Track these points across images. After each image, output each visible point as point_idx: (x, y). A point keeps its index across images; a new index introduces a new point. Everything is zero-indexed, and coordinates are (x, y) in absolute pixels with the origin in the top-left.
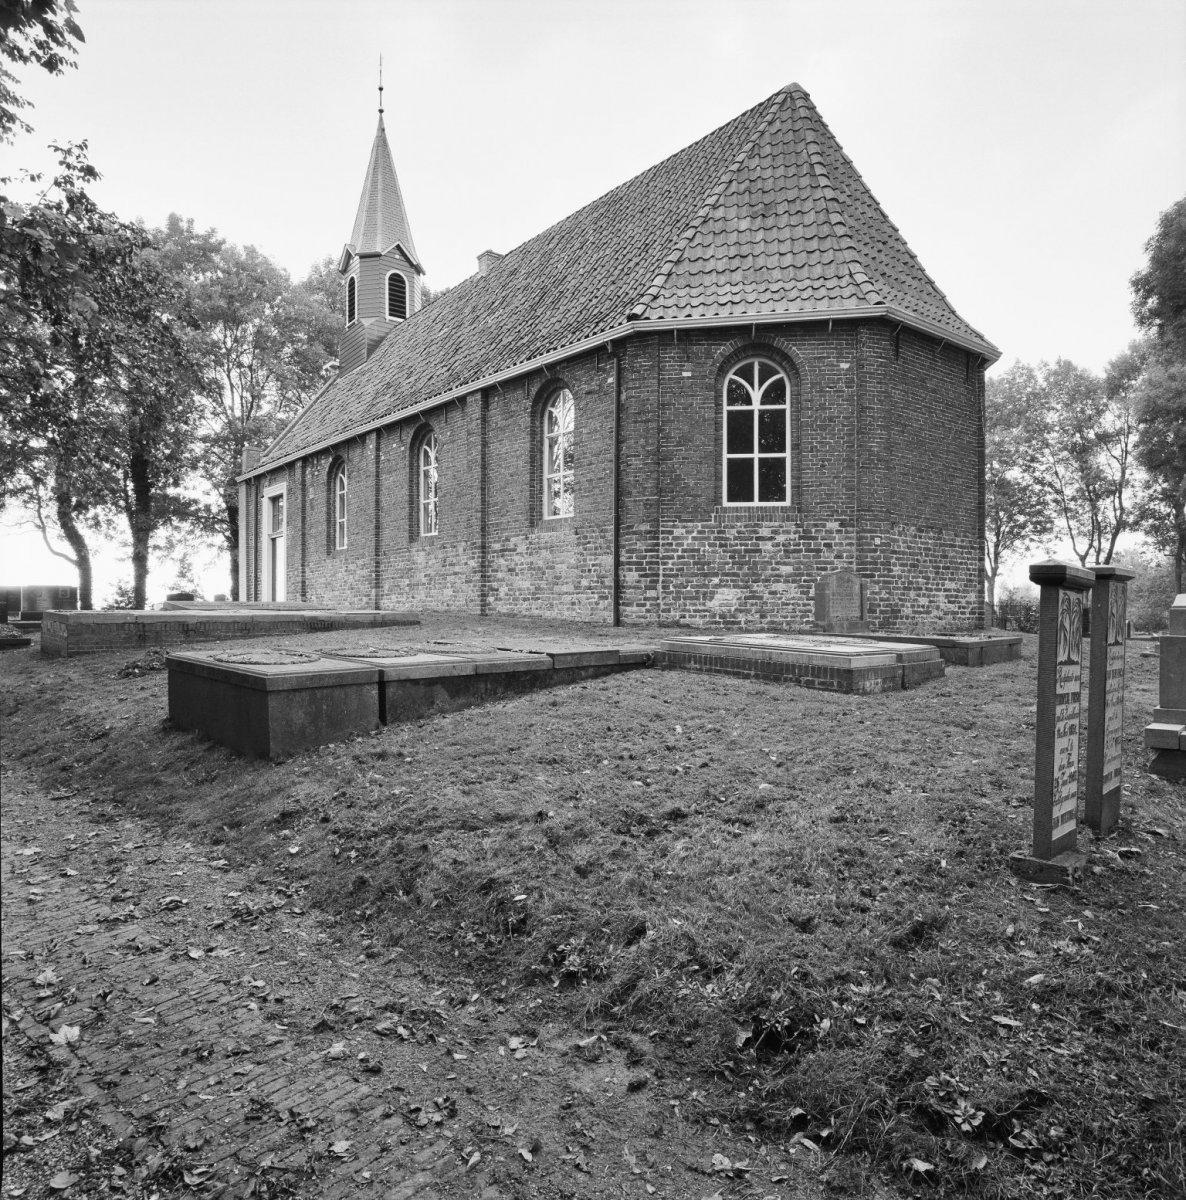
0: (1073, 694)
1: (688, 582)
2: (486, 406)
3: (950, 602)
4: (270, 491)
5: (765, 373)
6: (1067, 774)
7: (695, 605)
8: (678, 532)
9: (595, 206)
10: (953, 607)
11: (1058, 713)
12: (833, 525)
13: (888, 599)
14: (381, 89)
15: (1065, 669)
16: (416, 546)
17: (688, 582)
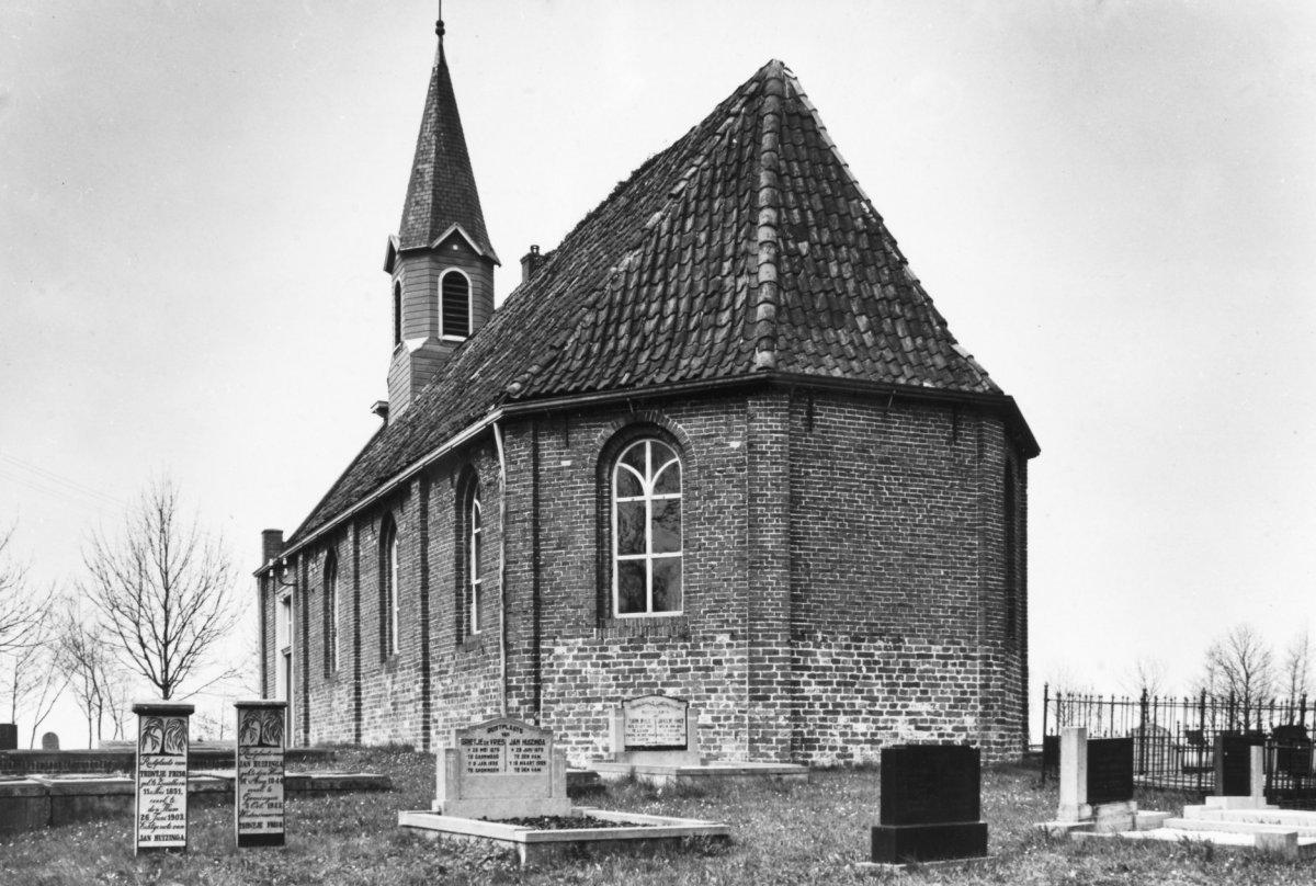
1: (570, 709)
3: (918, 728)
8: (559, 650)
12: (724, 639)
17: (570, 709)
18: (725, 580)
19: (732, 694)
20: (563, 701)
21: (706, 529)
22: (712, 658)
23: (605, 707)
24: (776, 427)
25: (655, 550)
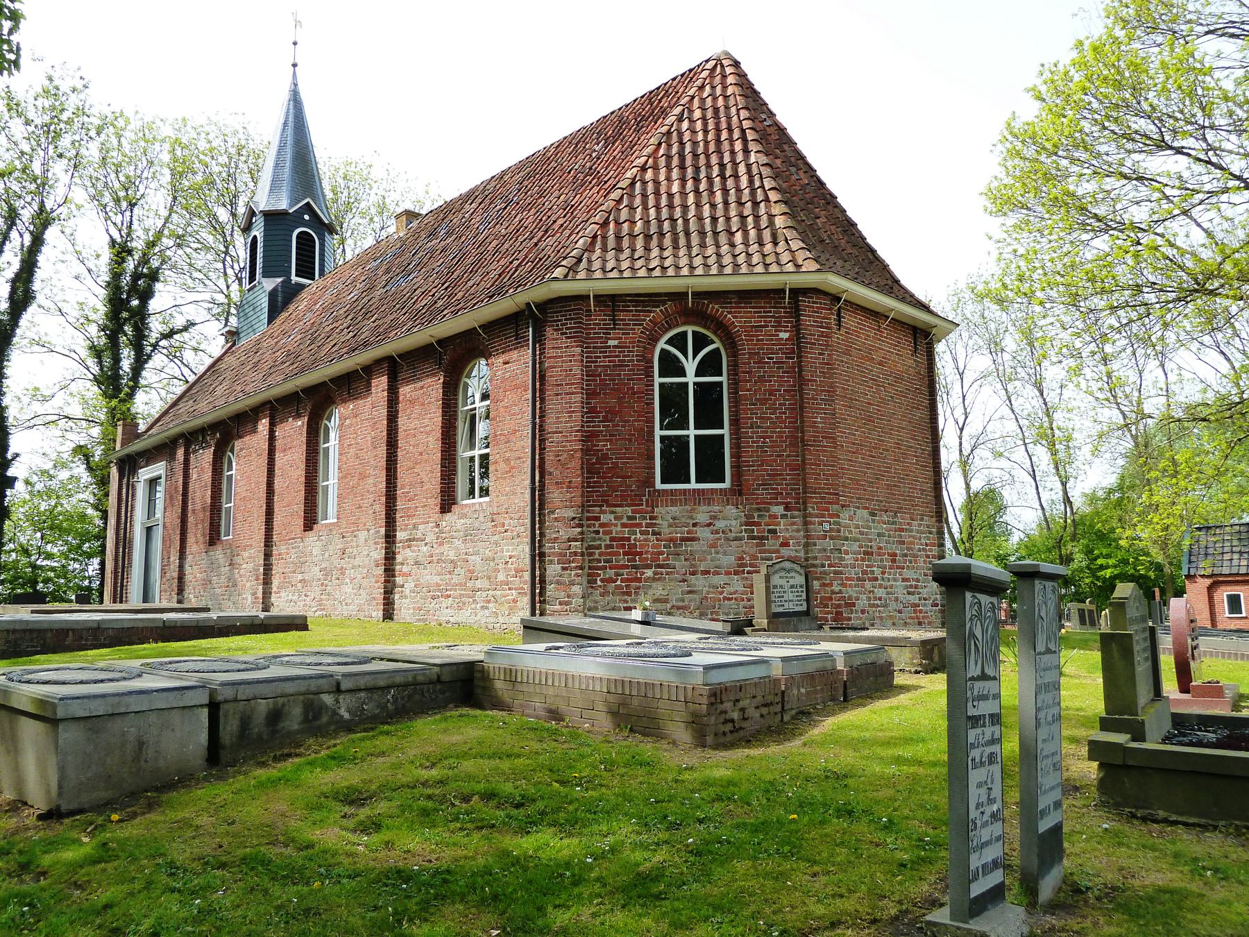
0: (992, 716)
3: (909, 593)
4: (145, 474)
5: (700, 342)
6: (988, 813)
7: (626, 601)
9: (521, 166)
10: (914, 599)
11: (971, 739)
12: (778, 510)
13: (840, 592)
14: (295, 44)
15: (978, 685)
16: (311, 537)
18: (778, 456)
20: (610, 568)
21: (758, 409)
22: (767, 528)
23: (655, 573)
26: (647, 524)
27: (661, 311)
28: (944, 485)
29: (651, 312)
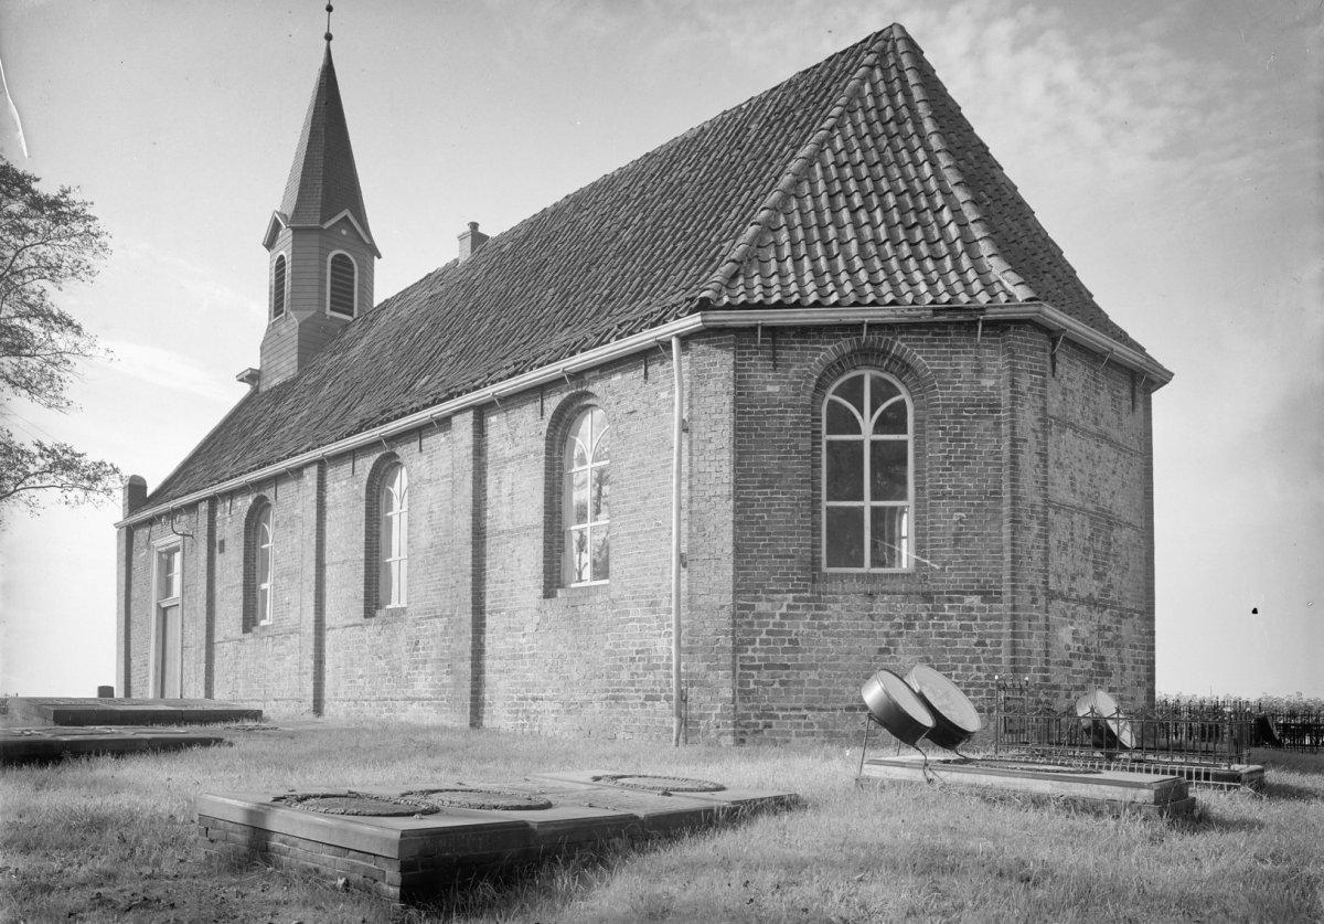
2: (480, 430)
14: (329, 9)
19: (983, 664)
24: (1036, 367)
25: (875, 497)
26: (781, 615)
27: (834, 349)
28: (897, 523)
29: (820, 349)
